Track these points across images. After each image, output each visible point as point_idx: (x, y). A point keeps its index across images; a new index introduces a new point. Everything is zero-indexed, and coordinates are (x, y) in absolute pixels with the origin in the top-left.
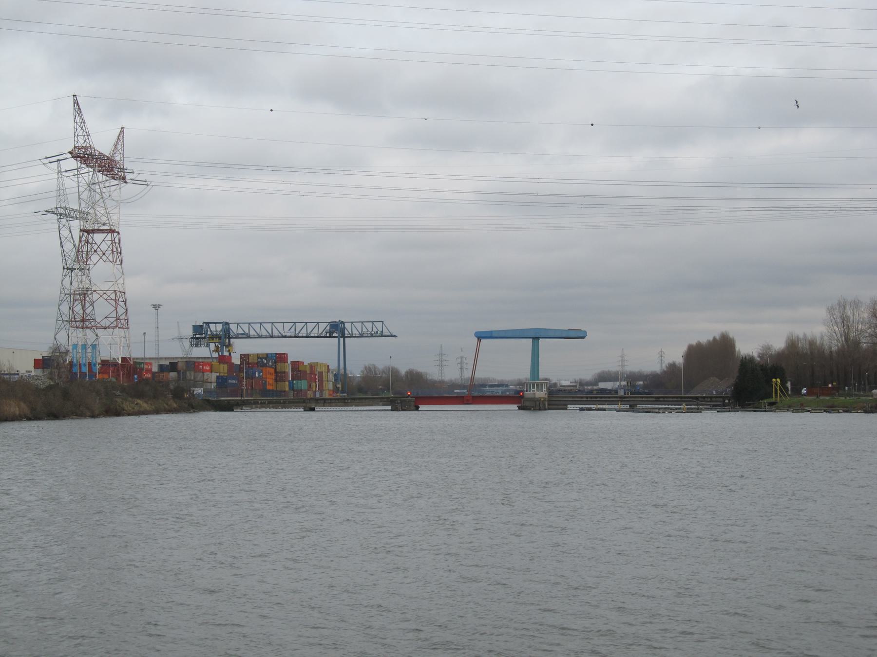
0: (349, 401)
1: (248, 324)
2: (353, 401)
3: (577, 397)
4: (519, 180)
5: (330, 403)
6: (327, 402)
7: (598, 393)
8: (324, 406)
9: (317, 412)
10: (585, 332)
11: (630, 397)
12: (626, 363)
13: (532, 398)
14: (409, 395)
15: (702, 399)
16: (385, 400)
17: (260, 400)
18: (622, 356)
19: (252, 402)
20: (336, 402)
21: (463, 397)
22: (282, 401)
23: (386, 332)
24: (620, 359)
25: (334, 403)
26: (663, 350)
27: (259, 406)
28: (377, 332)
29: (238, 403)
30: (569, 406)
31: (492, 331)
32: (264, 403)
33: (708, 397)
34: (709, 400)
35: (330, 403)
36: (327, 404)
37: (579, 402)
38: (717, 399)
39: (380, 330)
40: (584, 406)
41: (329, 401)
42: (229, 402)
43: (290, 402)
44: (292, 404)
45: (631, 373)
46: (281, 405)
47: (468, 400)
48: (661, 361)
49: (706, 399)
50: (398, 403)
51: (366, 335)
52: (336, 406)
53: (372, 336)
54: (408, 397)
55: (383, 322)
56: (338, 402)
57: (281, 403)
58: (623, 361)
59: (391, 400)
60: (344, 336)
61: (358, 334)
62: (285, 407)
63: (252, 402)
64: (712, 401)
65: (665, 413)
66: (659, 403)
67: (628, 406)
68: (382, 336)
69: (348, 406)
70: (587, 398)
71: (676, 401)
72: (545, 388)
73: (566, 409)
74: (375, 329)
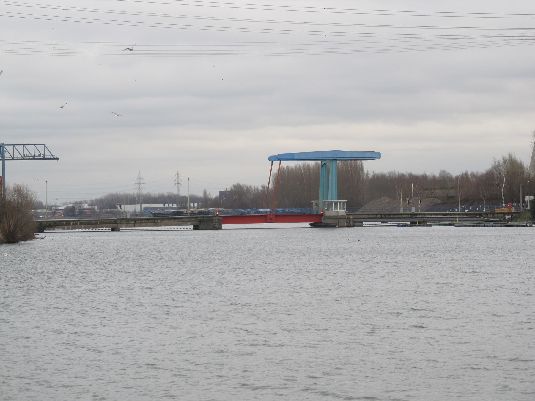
0: (159, 221)
1: (23, 146)
2: (162, 221)
3: (373, 215)
4: (428, 14)
5: (141, 223)
6: (137, 222)
7: (207, 213)
8: (134, 226)
9: (121, 232)
10: (379, 154)
11: (420, 214)
12: (142, 186)
13: (334, 216)
14: (217, 215)
15: (485, 216)
16: (193, 219)
17: (72, 221)
18: (139, 179)
19: (64, 223)
20: (146, 223)
21: (267, 216)
22: (93, 222)
23: (48, 155)
24: (137, 181)
25: (144, 223)
26: (179, 173)
27: (71, 227)
28: (40, 155)
29: (50, 224)
30: (364, 223)
31: (293, 153)
32: (76, 224)
33: (490, 214)
34: (492, 216)
35: (141, 223)
36: (138, 225)
37: (374, 220)
38: (499, 215)
39: (42, 153)
40: (401, 223)
41: (140, 221)
42: (41, 224)
43: (101, 223)
44: (103, 225)
45: (146, 195)
46: (92, 225)
47: (271, 219)
48: (178, 183)
49: (489, 215)
50: (215, 222)
51: (29, 158)
52: (146, 226)
53: (34, 159)
54: (215, 217)
55: (45, 145)
56: (149, 223)
57: (92, 224)
58: (139, 184)
59: (199, 219)
60: (3, 160)
61: (20, 157)
62: (75, 228)
63: (64, 223)
64: (495, 217)
65: (532, 226)
66: (446, 219)
67: (110, 229)
68: (44, 159)
69: (157, 226)
70: (381, 215)
71: (465, 217)
72: (345, 207)
73: (362, 226)
74: (37, 152)
